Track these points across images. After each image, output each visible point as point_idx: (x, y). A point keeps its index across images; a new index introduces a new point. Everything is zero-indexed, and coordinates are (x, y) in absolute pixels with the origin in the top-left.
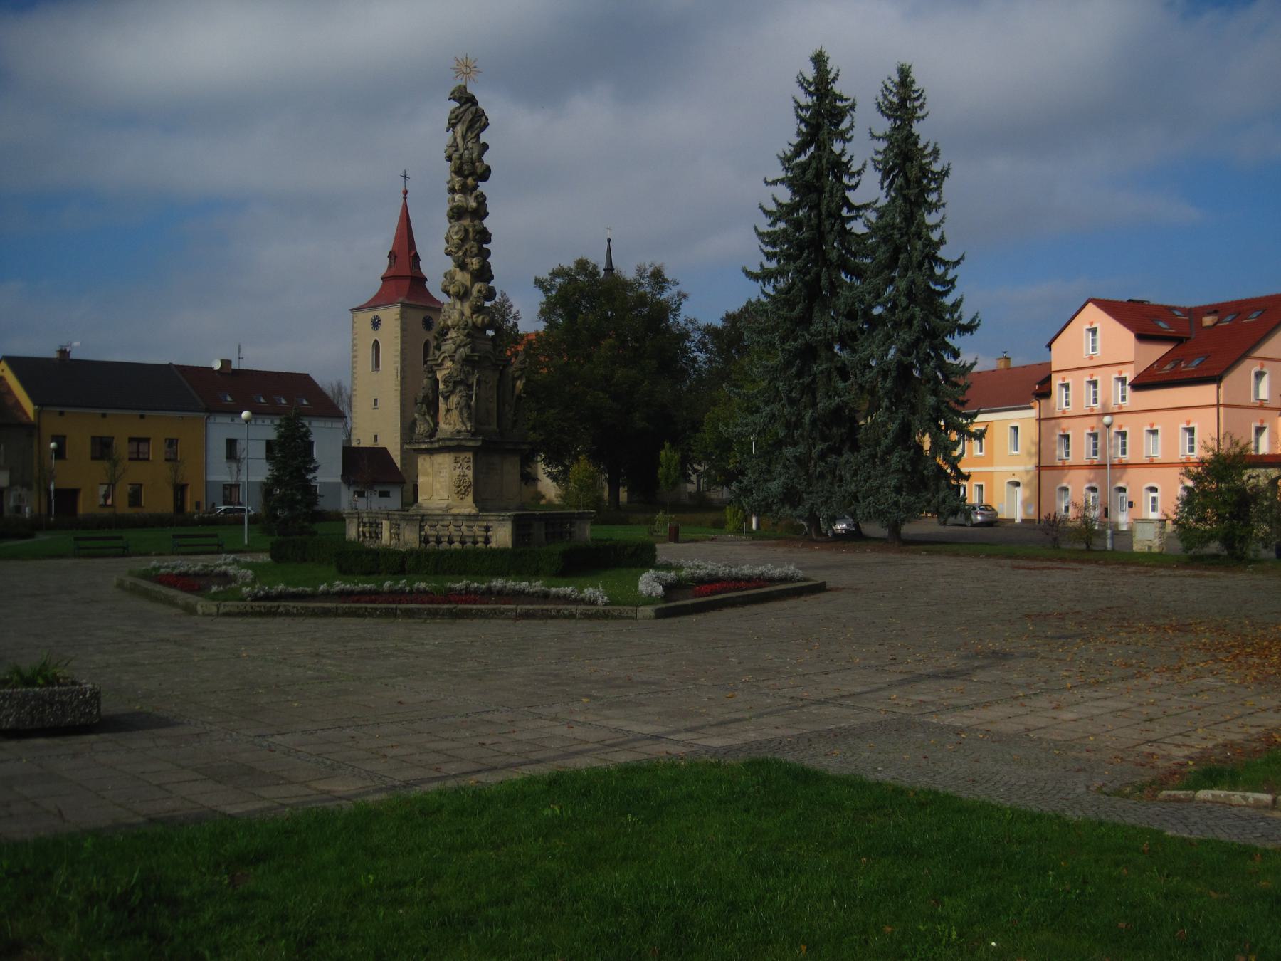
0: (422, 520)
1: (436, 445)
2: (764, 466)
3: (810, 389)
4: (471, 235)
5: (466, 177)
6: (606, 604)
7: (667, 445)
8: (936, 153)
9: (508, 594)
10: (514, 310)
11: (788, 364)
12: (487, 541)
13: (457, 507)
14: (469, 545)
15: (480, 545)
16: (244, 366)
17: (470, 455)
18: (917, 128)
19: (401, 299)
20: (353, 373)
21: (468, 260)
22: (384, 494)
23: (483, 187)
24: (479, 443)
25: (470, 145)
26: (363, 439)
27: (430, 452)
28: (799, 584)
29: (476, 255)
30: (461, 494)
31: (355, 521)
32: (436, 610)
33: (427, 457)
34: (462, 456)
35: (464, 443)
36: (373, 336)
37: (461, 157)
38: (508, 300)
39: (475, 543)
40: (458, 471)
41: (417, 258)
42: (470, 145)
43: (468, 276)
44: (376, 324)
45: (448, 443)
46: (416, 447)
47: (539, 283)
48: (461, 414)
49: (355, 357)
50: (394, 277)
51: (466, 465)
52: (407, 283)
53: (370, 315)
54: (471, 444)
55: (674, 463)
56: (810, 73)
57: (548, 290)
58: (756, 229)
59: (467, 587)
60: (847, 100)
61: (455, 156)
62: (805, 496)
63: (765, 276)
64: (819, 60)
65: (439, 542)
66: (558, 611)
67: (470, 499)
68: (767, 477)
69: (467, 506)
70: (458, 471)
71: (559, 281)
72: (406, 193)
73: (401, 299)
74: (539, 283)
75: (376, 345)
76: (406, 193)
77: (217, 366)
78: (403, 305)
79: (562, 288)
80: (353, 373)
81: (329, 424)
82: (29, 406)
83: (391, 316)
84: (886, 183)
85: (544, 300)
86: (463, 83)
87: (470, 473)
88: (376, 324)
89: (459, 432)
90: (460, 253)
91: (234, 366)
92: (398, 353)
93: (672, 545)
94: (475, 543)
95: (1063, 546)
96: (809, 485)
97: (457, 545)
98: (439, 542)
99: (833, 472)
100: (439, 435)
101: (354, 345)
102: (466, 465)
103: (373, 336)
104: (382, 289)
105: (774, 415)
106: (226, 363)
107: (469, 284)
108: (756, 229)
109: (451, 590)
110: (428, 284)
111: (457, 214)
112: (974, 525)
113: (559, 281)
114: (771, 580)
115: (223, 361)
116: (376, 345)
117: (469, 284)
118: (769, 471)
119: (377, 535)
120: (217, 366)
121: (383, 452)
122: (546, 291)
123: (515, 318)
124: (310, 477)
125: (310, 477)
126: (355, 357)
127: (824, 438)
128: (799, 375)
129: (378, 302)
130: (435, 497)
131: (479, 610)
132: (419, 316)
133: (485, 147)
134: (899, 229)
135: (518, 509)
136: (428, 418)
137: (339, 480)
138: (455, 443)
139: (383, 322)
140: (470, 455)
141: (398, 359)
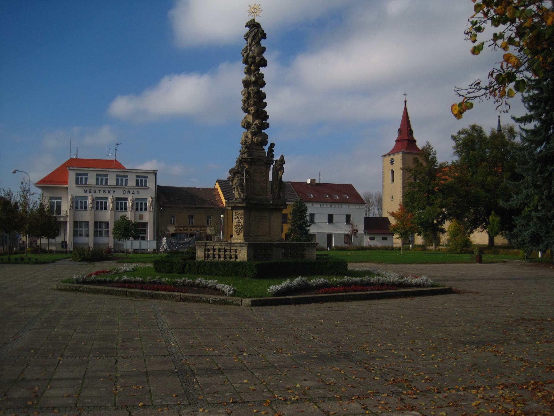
4: (252, 96)
5: (251, 65)
6: (231, 295)
7: (493, 213)
9: (387, 285)
10: (433, 150)
12: (236, 258)
15: (228, 259)
16: (322, 182)
19: (402, 150)
20: (383, 184)
21: (250, 109)
23: (262, 70)
24: (244, 205)
25: (253, 48)
28: (425, 289)
29: (254, 105)
32: (143, 293)
34: (239, 212)
35: (238, 205)
36: (391, 167)
37: (248, 55)
39: (231, 258)
41: (411, 132)
42: (253, 48)
44: (392, 162)
47: (453, 138)
49: (384, 177)
53: (390, 158)
54: (241, 205)
55: (496, 222)
59: (184, 282)
61: (245, 55)
62: (544, 239)
66: (201, 298)
67: (242, 235)
71: (462, 136)
72: (406, 102)
73: (402, 150)
75: (392, 171)
76: (406, 102)
77: (309, 181)
78: (403, 153)
79: (465, 139)
80: (383, 184)
81: (358, 207)
82: (224, 201)
83: (398, 158)
86: (253, 18)
87: (242, 221)
88: (392, 162)
91: (317, 181)
93: (478, 264)
95: (151, 265)
96: (548, 232)
97: (222, 259)
101: (383, 172)
103: (391, 167)
104: (396, 145)
105: (528, 195)
106: (313, 181)
107: (251, 121)
109: (177, 283)
110: (417, 143)
111: (246, 84)
113: (462, 136)
114: (410, 286)
115: (311, 180)
116: (392, 171)
117: (251, 121)
118: (528, 225)
120: (309, 181)
123: (435, 154)
124: (307, 228)
125: (307, 228)
126: (384, 177)
128: (541, 172)
129: (394, 152)
131: (162, 295)
133: (264, 49)
135: (279, 241)
140: (242, 211)
141: (401, 178)
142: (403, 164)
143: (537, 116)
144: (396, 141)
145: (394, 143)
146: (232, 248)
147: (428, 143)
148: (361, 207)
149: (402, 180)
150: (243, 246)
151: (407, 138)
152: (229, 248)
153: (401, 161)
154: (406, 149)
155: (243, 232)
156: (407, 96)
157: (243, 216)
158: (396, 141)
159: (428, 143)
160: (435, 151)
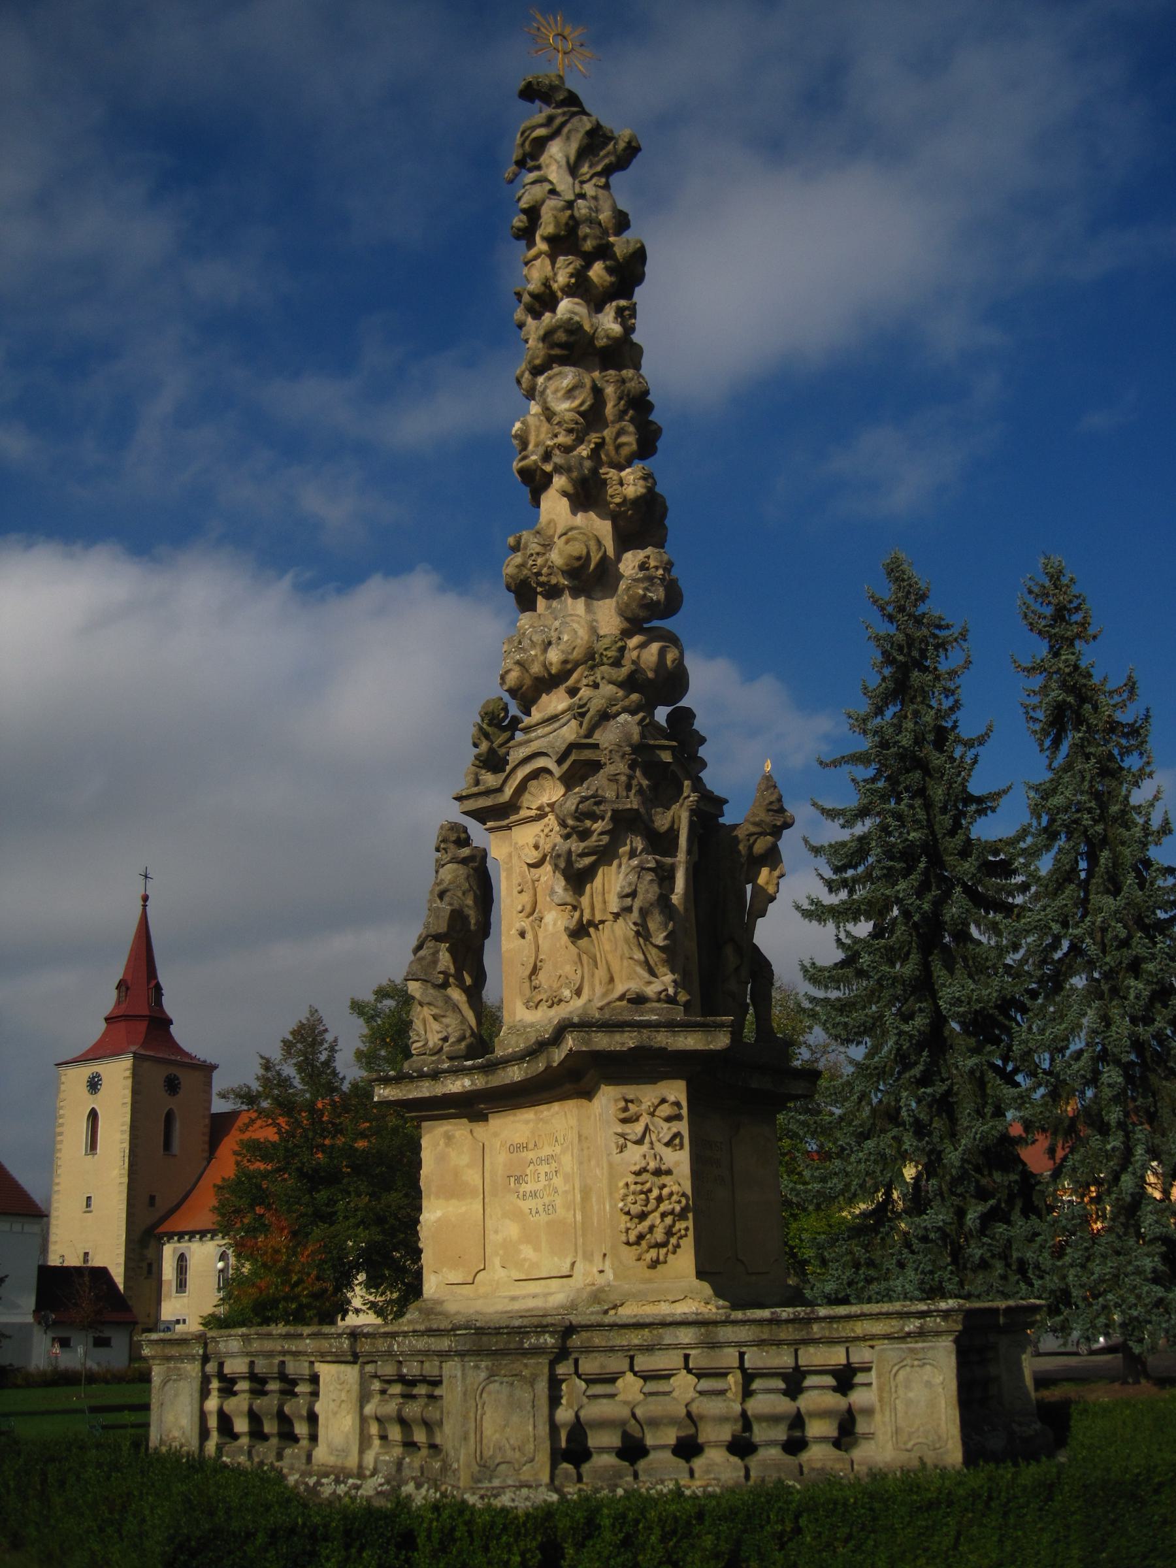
0: (562, 1353)
1: (515, 1074)
2: (858, 1251)
3: (945, 1105)
4: (610, 410)
5: (589, 259)
8: (1131, 687)
10: (329, 1037)
11: (903, 1059)
12: (847, 1431)
13: (639, 1297)
14: (769, 1455)
15: (818, 1455)
17: (676, 1091)
18: (1088, 655)
19: (133, 1048)
22: (102, 1342)
26: (65, 1249)
27: (472, 1108)
30: (652, 1247)
31: (193, 1369)
33: (459, 1129)
34: (648, 1095)
38: (320, 1020)
40: (635, 1156)
41: (158, 989)
43: (603, 528)
44: (94, 1084)
45: (602, 1042)
46: (425, 1090)
47: (358, 1007)
48: (642, 933)
50: (125, 1017)
51: (666, 1130)
52: (142, 1027)
53: (86, 1071)
54: (690, 1042)
56: (888, 592)
57: (373, 1017)
58: (806, 841)
60: (948, 627)
63: (840, 914)
64: (895, 572)
65: (632, 1450)
67: (684, 1261)
68: (872, 1272)
69: (679, 1289)
70: (635, 1156)
71: (389, 1003)
72: (145, 898)
73: (133, 1048)
74: (358, 1007)
75: (93, 1115)
76: (145, 898)
78: (136, 1057)
81: (17, 1227)
83: (118, 1073)
84: (1047, 743)
85: (366, 1031)
87: (680, 1160)
88: (94, 1084)
89: (639, 1000)
90: (584, 451)
92: (127, 1128)
94: (795, 1445)
98: (632, 1450)
99: (1005, 1257)
100: (507, 1043)
102: (666, 1130)
104: (119, 997)
108: (806, 841)
110: (173, 1029)
112: (1092, 1353)
116: (93, 1115)
119: (290, 1428)
121: (102, 1274)
122: (370, 1019)
123: (332, 1049)
127: (982, 1195)
130: (497, 1273)
132: (158, 1075)
134: (1090, 811)
136: (456, 995)
137: (30, 1319)
138: (626, 1041)
139: (104, 1082)
140: (676, 1091)
141: (127, 1137)
142: (211, 1078)
143: (875, 909)
144: (106, 1019)
145: (102, 1026)
146: (812, 1356)
147: (313, 1012)
148: (27, 1228)
149: (126, 1145)
150: (921, 1334)
151: (146, 1012)
152: (784, 1359)
153: (129, 1082)
154: (145, 1044)
155: (688, 1244)
156: (150, 883)
157: (683, 1127)
158: (106, 1019)
159: (313, 1012)
160: (336, 1040)
